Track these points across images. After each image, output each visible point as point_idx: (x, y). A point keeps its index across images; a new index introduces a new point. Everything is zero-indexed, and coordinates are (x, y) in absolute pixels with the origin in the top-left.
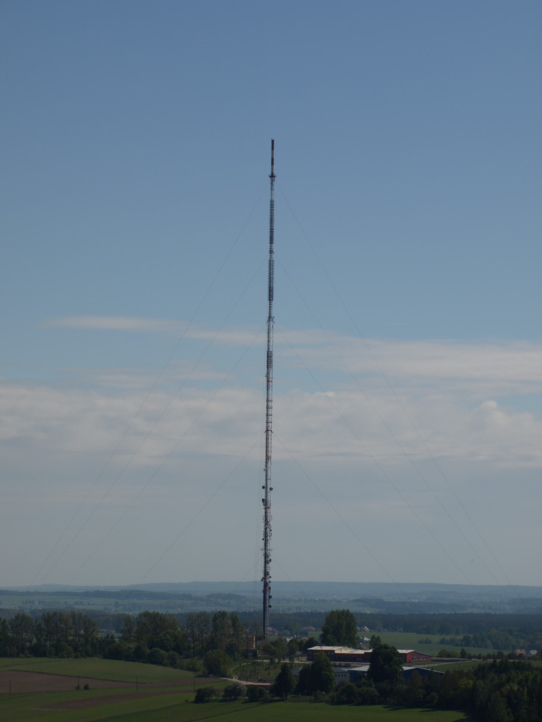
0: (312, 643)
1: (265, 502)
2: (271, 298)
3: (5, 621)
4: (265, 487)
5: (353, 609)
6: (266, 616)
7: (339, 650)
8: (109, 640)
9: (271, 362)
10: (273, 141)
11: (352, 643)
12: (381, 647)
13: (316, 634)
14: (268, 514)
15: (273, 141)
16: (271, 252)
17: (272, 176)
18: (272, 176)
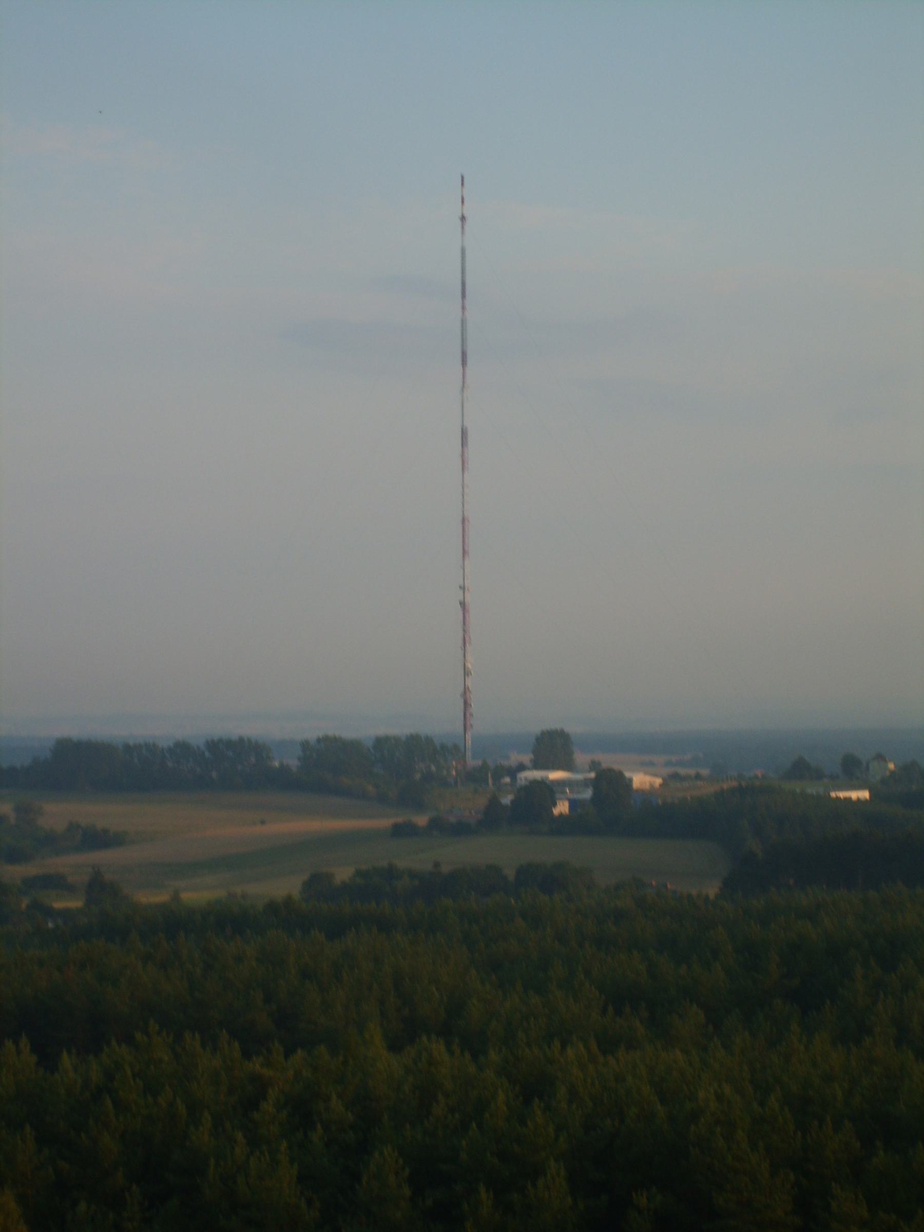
0: (522, 767)
1: (463, 604)
2: (464, 362)
3: (163, 750)
4: (463, 587)
5: (571, 729)
6: (467, 755)
7: (556, 775)
8: (284, 769)
9: (466, 439)
10: (463, 178)
11: (568, 766)
12: (590, 768)
13: (526, 758)
14: (466, 454)
15: (463, 178)
16: (463, 308)
17: (463, 218)
18: (463, 218)
